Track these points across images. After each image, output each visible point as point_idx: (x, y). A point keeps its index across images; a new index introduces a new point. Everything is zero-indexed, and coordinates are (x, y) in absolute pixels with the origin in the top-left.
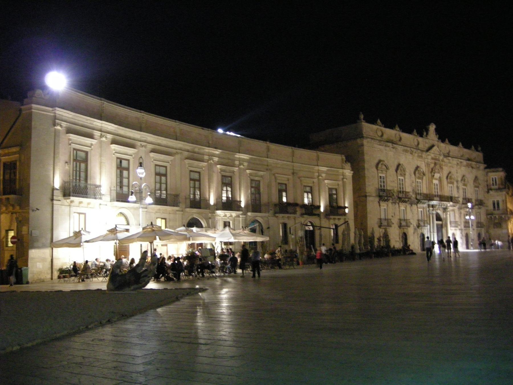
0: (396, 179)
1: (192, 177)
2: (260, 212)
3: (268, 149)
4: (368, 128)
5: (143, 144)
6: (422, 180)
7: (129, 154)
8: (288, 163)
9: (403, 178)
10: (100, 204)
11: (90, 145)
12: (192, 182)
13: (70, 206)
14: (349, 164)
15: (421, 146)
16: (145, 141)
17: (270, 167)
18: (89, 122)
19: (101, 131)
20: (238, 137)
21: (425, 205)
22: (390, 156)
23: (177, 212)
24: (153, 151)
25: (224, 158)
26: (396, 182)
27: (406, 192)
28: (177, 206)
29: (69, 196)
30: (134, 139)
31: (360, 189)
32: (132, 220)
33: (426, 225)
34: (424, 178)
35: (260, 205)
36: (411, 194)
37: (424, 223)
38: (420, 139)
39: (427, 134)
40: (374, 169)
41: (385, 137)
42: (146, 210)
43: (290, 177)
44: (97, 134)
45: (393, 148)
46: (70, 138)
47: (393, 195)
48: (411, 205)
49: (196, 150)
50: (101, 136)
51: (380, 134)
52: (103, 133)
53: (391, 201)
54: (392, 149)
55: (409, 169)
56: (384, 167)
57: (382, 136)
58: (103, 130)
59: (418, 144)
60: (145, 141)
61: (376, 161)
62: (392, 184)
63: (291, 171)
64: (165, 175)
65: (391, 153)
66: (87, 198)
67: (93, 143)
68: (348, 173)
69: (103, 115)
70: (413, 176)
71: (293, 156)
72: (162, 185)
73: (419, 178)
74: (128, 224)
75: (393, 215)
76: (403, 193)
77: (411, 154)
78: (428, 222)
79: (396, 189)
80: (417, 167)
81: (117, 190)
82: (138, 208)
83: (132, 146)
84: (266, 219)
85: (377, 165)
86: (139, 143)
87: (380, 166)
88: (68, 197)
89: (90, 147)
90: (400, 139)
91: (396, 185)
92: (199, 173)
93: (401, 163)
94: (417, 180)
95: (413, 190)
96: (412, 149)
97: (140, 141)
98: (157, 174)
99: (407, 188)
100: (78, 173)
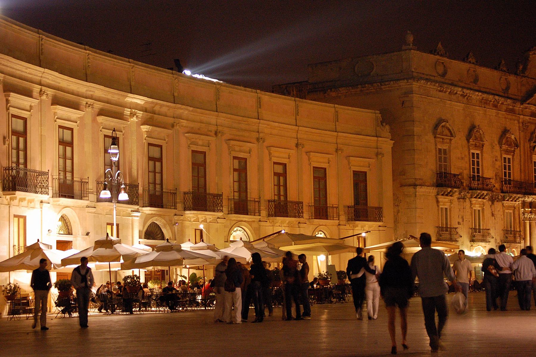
0: (467, 153)
1: (151, 155)
2: (247, 215)
3: (259, 102)
4: (420, 60)
5: (90, 101)
6: (513, 156)
7: (72, 119)
8: (290, 127)
9: (478, 152)
10: (42, 202)
11: (28, 108)
12: (151, 163)
13: (9, 205)
14: (387, 127)
15: (513, 91)
16: (91, 98)
17: (261, 135)
18: (28, 71)
19: (40, 84)
20: (212, 82)
21: (518, 203)
22: (456, 110)
23: (219, 220)
24: (102, 113)
25: (194, 121)
26: (467, 159)
27: (483, 177)
28: (380, 221)
29: (14, 189)
30: (78, 95)
31: (403, 173)
32: (77, 228)
33: (518, 240)
34: (517, 151)
35: (71, 186)
36: (493, 181)
37: (515, 237)
38: (512, 78)
39: (525, 69)
40: (430, 137)
41: (450, 75)
42: (93, 210)
43: (293, 152)
44: (36, 89)
45: (463, 96)
46: (56, 111)
47: (462, 183)
48: (493, 203)
49: (157, 108)
50: (41, 93)
51: (440, 69)
52: (43, 88)
53: (456, 195)
54: (461, 98)
55: (490, 136)
56: (446, 132)
57: (444, 75)
58: (175, 116)
59: (508, 88)
60: (91, 98)
61: (434, 121)
62: (459, 165)
63: (295, 141)
64: (160, 160)
65: (459, 107)
66: (26, 191)
67: (33, 104)
68: (387, 145)
69: (42, 57)
70: (497, 147)
71: (297, 114)
72: (157, 174)
73: (507, 152)
74: (70, 233)
75: (461, 220)
76: (478, 180)
77: (495, 106)
78: (522, 233)
79: (466, 173)
80: (505, 132)
81: (59, 179)
82: (81, 208)
83: (75, 106)
84: (255, 225)
85: (436, 126)
86: (84, 101)
87: (440, 129)
88: (13, 192)
89: (30, 111)
90: (476, 80)
91: (467, 166)
92: (25, 120)
93: (477, 123)
94: (504, 156)
95: (496, 175)
96: (497, 97)
97: (86, 98)
98: (150, 159)
99: (485, 171)
100: (21, 153)
